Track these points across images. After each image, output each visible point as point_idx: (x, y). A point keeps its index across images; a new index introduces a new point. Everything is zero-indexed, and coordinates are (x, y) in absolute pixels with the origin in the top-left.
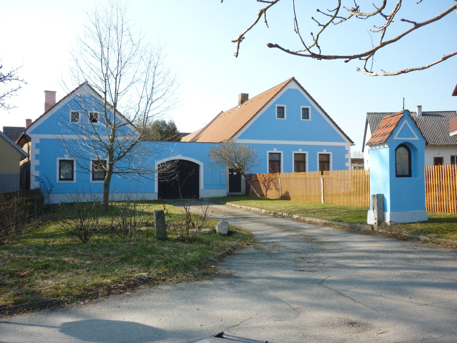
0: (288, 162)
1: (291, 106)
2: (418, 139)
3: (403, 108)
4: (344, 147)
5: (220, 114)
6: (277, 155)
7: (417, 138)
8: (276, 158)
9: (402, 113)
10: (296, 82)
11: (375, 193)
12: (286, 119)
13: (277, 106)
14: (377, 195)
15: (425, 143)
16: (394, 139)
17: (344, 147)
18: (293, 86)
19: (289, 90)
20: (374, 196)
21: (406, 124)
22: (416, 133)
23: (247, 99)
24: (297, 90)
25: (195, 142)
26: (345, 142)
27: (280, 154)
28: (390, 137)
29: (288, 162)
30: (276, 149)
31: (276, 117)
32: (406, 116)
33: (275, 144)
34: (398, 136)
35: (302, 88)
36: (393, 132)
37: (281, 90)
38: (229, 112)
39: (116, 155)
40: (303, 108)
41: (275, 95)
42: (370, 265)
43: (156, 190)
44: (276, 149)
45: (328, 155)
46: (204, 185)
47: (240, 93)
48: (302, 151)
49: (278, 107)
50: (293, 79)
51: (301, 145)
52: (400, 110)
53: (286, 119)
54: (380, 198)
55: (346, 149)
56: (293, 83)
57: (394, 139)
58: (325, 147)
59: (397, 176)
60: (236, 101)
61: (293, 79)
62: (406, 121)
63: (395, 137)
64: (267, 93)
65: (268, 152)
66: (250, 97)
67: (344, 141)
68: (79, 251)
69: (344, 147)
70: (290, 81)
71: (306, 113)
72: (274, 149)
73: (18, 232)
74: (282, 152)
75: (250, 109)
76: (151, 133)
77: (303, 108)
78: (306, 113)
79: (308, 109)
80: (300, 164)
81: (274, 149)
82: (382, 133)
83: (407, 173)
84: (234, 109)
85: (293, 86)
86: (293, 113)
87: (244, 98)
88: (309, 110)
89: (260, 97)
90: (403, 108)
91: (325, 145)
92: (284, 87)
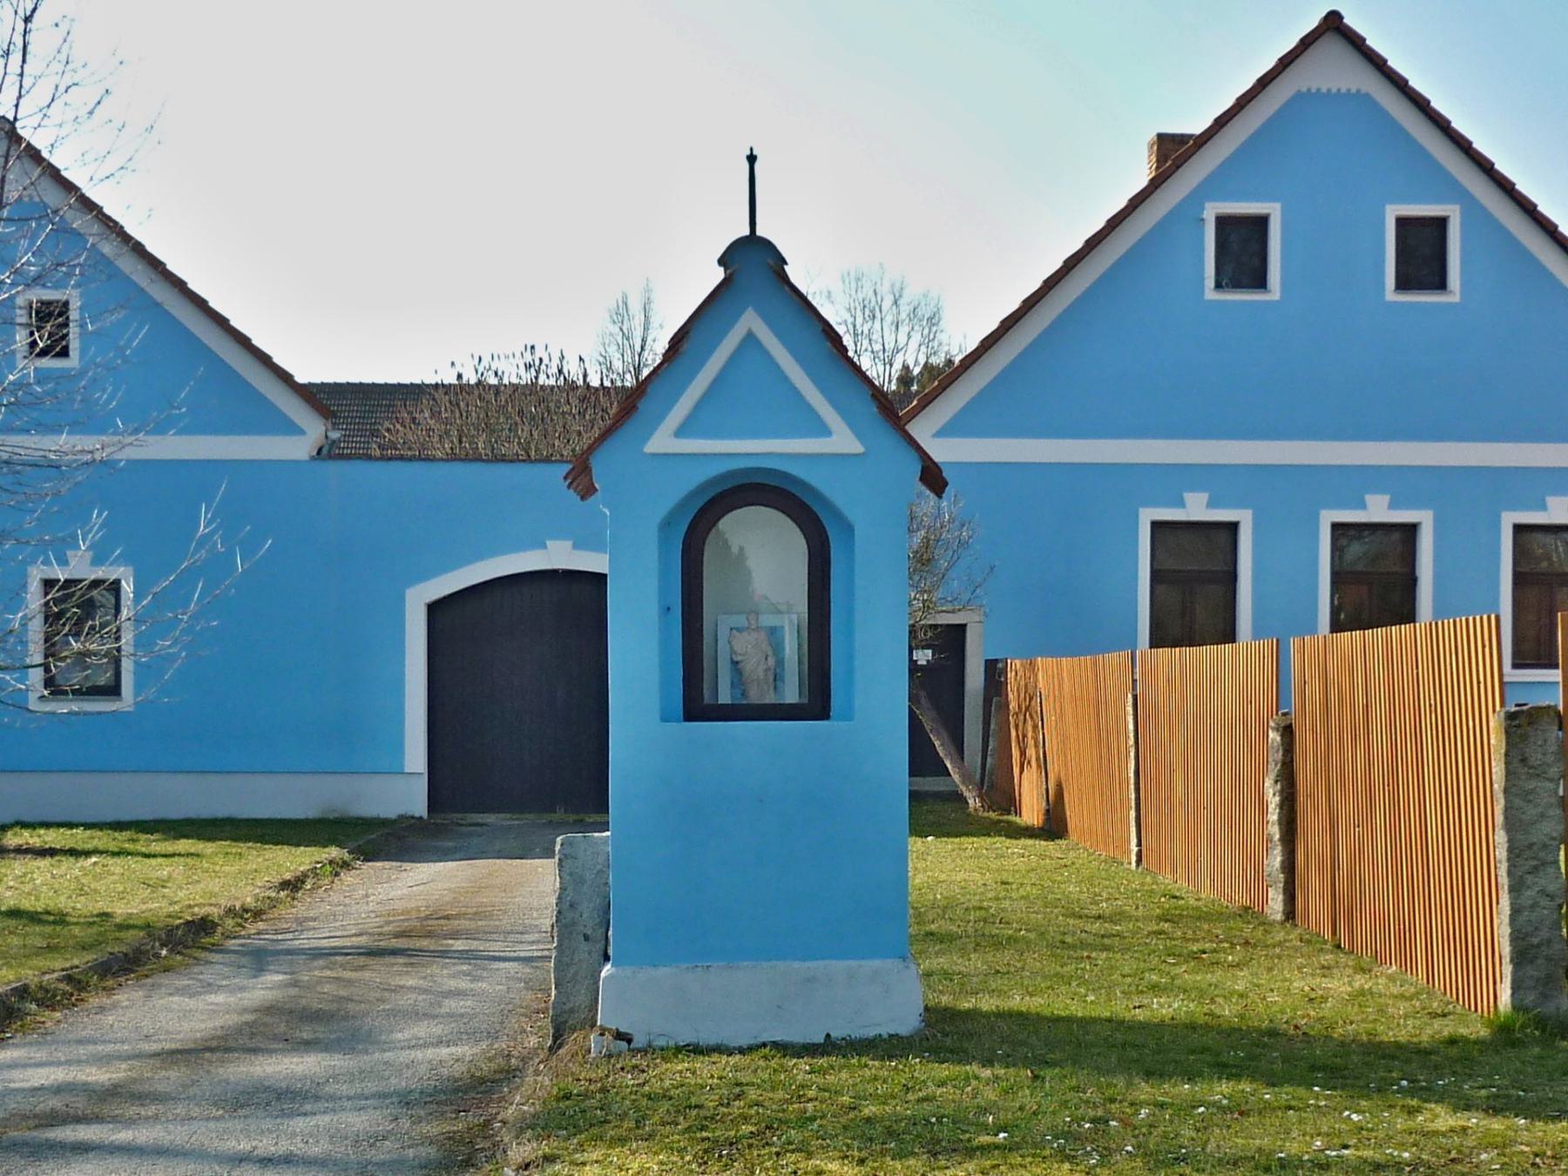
0: (1283, 573)
2: (859, 448)
7: (842, 440)
10: (1356, 42)
15: (916, 468)
18: (1333, 72)
19: (1299, 98)
21: (750, 337)
24: (1364, 98)
29: (1283, 573)
31: (1210, 282)
33: (1196, 468)
44: (1204, 497)
47: (1151, 136)
48: (1212, 504)
49: (1223, 222)
50: (1333, 23)
61: (1333, 23)
68: (1458, 1068)
74: (1244, 517)
76: (335, 435)
80: (1195, 588)
83: (791, 694)
86: (1329, 244)
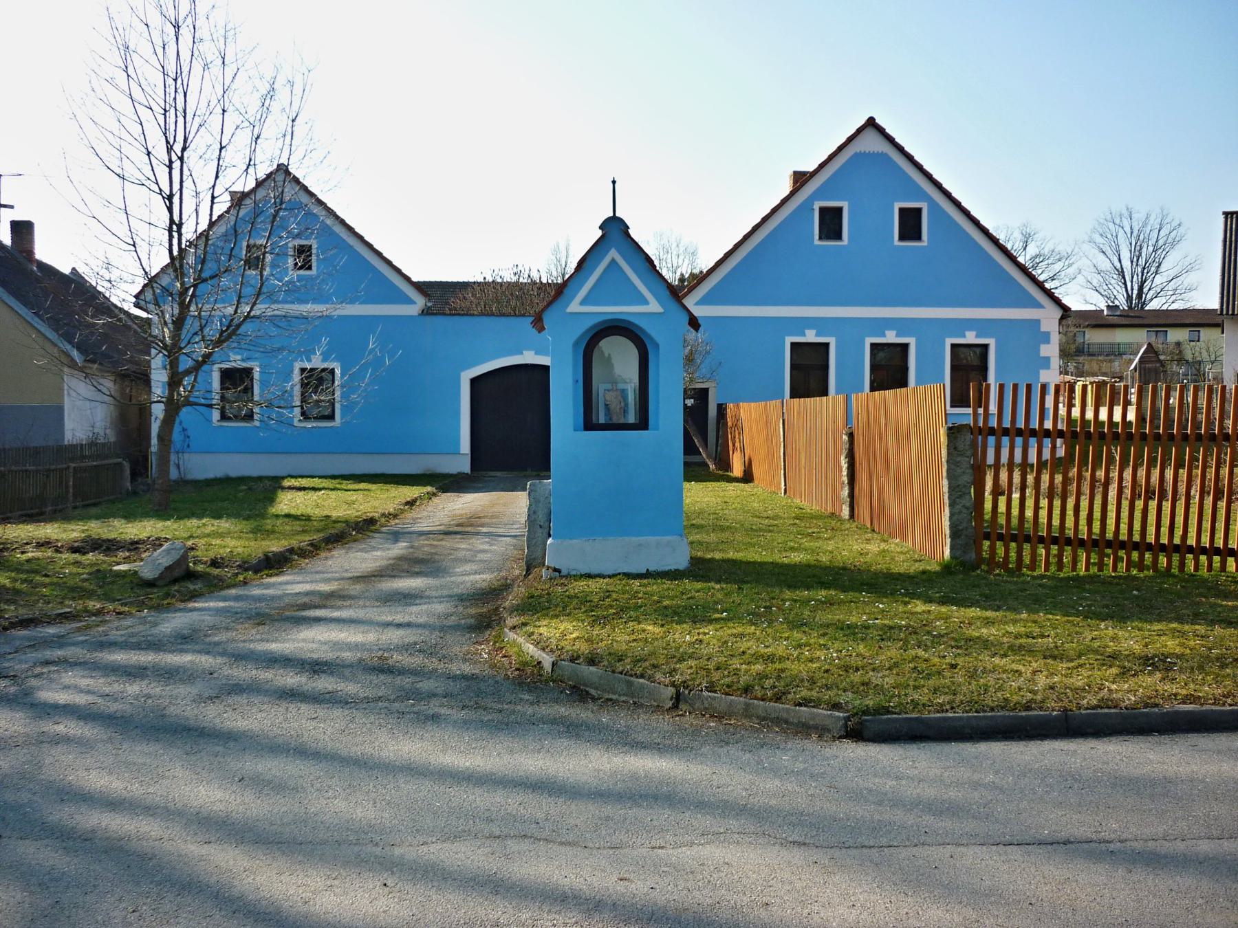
2: (661, 310)
7: (654, 306)
8: (972, 358)
10: (881, 131)
12: (925, 244)
15: (686, 319)
16: (569, 310)
18: (870, 143)
19: (856, 155)
21: (613, 260)
26: (1040, 306)
29: (849, 366)
30: (814, 332)
31: (817, 237)
33: (810, 318)
35: (900, 149)
36: (566, 291)
39: (185, 363)
42: (1129, 692)
43: (465, 446)
44: (814, 332)
47: (791, 173)
50: (871, 122)
51: (891, 319)
53: (925, 244)
55: (1042, 329)
56: (871, 134)
57: (569, 310)
62: (613, 254)
65: (869, 340)
71: (910, 224)
72: (807, 332)
76: (429, 304)
78: (910, 224)
81: (807, 332)
86: (870, 221)
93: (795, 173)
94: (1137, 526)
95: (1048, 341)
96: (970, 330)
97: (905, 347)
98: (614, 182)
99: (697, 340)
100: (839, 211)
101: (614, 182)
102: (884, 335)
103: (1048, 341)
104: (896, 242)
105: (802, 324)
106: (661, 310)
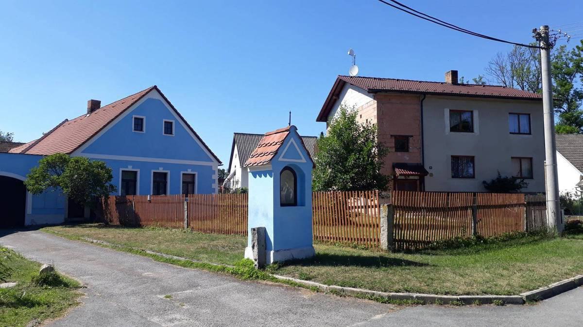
1: (150, 117)
2: (306, 162)
3: (290, 124)
4: (211, 167)
5: (64, 122)
6: (190, 176)
7: (304, 160)
8: (189, 179)
9: (286, 131)
10: (159, 91)
11: (256, 226)
13: (134, 116)
14: (259, 229)
15: (312, 166)
17: (212, 166)
18: (154, 95)
19: (149, 99)
20: (254, 230)
22: (304, 156)
23: (99, 107)
25: (7, 153)
27: (136, 172)
28: (275, 157)
29: (174, 183)
30: (131, 167)
32: (293, 133)
34: (283, 157)
37: (140, 99)
38: (75, 121)
40: (165, 122)
41: (132, 104)
44: (131, 167)
45: (194, 175)
46: (33, 209)
50: (155, 87)
52: (287, 126)
54: (261, 233)
56: (154, 91)
58: (161, 165)
59: (282, 205)
60: (84, 109)
61: (155, 87)
62: (292, 140)
63: (281, 159)
64: (123, 101)
66: (102, 105)
67: (211, 161)
69: (212, 166)
70: (151, 90)
71: (169, 128)
73: (246, 279)
74: (169, 172)
75: (100, 119)
77: (165, 122)
78: (169, 128)
79: (171, 123)
82: (269, 152)
84: (81, 118)
85: (154, 95)
86: (153, 125)
87: (95, 105)
88: (173, 125)
89: (114, 105)
90: (290, 124)
91: (190, 164)
92: (144, 96)
93: (100, 102)
94: (421, 238)
95: (214, 174)
96: (189, 168)
97: (136, 172)
98: (290, 113)
99: (68, 166)
100: (142, 119)
101: (290, 113)
102: (187, 171)
103: (214, 174)
104: (163, 134)
105: (186, 167)
106: (306, 162)
